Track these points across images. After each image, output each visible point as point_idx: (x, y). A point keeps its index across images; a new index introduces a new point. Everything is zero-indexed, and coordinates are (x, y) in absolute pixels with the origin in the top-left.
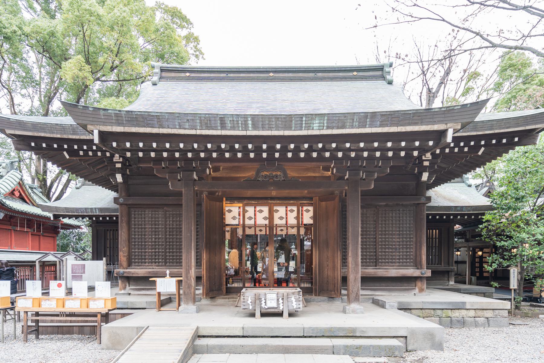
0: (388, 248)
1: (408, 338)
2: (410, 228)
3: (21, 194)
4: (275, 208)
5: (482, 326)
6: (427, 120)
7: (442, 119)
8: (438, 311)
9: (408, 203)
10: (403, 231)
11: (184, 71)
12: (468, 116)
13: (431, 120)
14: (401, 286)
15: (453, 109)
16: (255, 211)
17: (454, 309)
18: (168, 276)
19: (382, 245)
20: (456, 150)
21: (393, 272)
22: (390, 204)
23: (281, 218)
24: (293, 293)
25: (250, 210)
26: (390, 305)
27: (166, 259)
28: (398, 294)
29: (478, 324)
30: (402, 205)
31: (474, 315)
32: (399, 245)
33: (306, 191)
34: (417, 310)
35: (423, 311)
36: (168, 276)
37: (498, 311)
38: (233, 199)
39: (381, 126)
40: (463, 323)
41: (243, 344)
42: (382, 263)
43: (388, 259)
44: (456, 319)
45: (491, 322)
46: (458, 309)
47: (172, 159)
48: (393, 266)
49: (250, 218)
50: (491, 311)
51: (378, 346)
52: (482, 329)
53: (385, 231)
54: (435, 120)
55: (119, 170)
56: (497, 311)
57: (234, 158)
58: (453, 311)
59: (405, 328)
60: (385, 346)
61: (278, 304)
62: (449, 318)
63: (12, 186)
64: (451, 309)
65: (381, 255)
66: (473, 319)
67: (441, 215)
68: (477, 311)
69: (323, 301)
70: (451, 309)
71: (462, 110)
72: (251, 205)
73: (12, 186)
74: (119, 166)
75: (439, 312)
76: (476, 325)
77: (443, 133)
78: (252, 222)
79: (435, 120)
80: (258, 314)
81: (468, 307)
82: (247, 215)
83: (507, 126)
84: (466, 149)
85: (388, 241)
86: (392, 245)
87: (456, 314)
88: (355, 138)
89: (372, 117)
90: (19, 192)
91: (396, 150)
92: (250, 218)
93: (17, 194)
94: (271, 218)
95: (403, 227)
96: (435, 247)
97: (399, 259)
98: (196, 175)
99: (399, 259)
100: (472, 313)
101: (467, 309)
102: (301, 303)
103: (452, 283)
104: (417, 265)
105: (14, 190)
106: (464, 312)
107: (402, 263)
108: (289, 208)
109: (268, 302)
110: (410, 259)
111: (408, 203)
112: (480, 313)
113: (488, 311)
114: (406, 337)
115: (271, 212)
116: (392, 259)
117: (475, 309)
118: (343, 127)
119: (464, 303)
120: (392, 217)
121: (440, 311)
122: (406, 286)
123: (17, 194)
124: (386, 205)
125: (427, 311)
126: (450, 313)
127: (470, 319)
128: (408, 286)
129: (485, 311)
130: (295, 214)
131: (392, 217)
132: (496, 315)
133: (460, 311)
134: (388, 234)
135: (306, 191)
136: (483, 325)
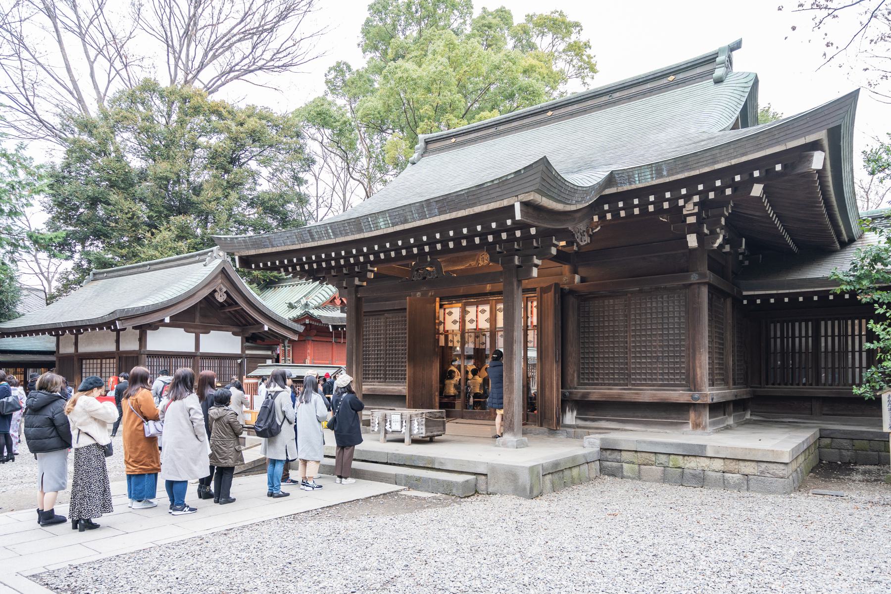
0: (645, 357)
2: (679, 324)
5: (735, 488)
6: (484, 198)
7: (499, 194)
8: (662, 456)
9: (675, 284)
10: (668, 329)
11: (544, 111)
12: (528, 185)
13: (489, 197)
14: (666, 418)
15: (507, 180)
17: (689, 456)
19: (635, 352)
20: (712, 195)
21: (647, 395)
22: (646, 288)
24: (416, 415)
25: (472, 310)
26: (589, 443)
27: (385, 374)
28: (643, 429)
29: (729, 483)
30: (665, 288)
31: (722, 468)
32: (662, 352)
33: (419, 294)
35: (639, 454)
37: (766, 464)
38: (452, 298)
39: (441, 213)
40: (701, 480)
41: (398, 472)
42: (635, 379)
43: (645, 374)
45: (751, 483)
46: (695, 456)
47: (339, 267)
48: (653, 385)
50: (753, 464)
51: (437, 480)
52: (735, 494)
53: (640, 330)
54: (493, 196)
55: (692, 229)
56: (764, 465)
57: (399, 256)
58: (686, 458)
59: (484, 463)
60: (444, 481)
62: (680, 470)
63: (331, 293)
64: (684, 456)
65: (634, 368)
66: (720, 474)
67: (808, 296)
68: (728, 462)
69: (543, 434)
70: (684, 456)
71: (517, 178)
72: (471, 304)
73: (331, 293)
74: (691, 220)
75: (663, 459)
76: (725, 485)
77: (512, 207)
78: (473, 326)
79: (493, 196)
80: (407, 440)
81: (710, 453)
82: (468, 318)
83: (741, 152)
84: (728, 192)
85: (645, 346)
86: (651, 352)
87: (692, 464)
88: (416, 232)
89: (427, 206)
91: (643, 206)
92: (471, 321)
95: (668, 324)
97: (662, 374)
99: (662, 374)
100: (718, 465)
101: (711, 458)
102: (424, 427)
103: (748, 416)
105: (335, 298)
106: (703, 463)
107: (645, 380)
108: (480, 308)
109: (393, 424)
110: (681, 374)
111: (675, 284)
112: (732, 466)
113: (747, 464)
115: (464, 312)
116: (651, 374)
117: (724, 459)
118: (406, 221)
119: (703, 447)
120: (651, 309)
121: (665, 456)
122: (675, 419)
124: (641, 291)
125: (643, 454)
128: (679, 418)
129: (742, 464)
130: (487, 315)
131: (651, 309)
132: (762, 472)
133: (698, 459)
134: (645, 336)
135: (419, 294)
136: (738, 487)
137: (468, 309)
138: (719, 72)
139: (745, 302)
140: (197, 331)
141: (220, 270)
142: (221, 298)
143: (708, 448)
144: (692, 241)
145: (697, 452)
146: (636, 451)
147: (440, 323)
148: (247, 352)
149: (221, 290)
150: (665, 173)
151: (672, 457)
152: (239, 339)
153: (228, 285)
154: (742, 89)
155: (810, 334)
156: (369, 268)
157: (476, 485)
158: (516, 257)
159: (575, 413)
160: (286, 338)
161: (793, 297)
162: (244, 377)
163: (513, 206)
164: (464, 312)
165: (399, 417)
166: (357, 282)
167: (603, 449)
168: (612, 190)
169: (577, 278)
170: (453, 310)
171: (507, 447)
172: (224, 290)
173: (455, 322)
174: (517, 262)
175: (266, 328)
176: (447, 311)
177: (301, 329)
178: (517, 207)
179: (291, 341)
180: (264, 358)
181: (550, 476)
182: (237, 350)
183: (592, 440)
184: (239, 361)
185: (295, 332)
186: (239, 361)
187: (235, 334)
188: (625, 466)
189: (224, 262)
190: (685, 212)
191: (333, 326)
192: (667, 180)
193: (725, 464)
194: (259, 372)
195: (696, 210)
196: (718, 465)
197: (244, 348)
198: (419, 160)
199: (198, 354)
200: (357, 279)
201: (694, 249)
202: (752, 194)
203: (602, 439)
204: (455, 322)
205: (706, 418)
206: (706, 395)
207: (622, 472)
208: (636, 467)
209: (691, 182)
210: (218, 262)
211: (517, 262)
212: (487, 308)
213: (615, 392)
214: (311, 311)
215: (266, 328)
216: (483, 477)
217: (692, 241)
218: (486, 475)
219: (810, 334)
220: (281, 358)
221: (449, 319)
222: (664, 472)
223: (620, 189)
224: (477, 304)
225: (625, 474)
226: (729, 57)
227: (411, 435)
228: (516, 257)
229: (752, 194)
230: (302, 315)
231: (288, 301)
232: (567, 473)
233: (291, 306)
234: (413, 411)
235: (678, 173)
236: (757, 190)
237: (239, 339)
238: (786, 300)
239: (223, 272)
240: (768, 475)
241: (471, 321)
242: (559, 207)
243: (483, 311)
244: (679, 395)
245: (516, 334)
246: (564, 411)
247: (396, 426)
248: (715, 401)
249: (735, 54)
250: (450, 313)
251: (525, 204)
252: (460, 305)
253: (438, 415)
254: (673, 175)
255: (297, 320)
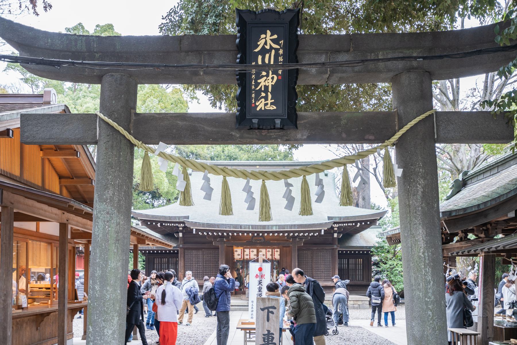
9: (480, 274)
82: (245, 253)
92: (247, 255)
108: (267, 250)
112: (356, 302)
115: (258, 252)
124: (317, 249)
130: (270, 253)
136: (357, 308)
137: (245, 250)
161: (346, 251)
164: (258, 252)
173: (239, 255)
204: (239, 255)
212: (255, 250)
241: (247, 255)
243: (253, 251)
246: (469, 239)
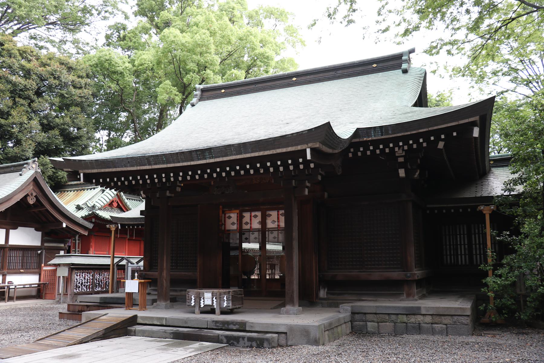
1: (288, 334)
3: (118, 204)
4: (268, 212)
8: (393, 316)
16: (278, 215)
17: (410, 314)
18: (136, 278)
21: (376, 275)
23: (274, 222)
25: (247, 215)
29: (435, 331)
34: (370, 315)
36: (136, 278)
38: (231, 207)
40: (418, 329)
44: (412, 325)
46: (414, 314)
49: (247, 223)
50: (449, 317)
55: (402, 165)
56: (455, 318)
59: (285, 325)
61: (213, 303)
62: (405, 324)
66: (430, 325)
68: (434, 317)
70: (407, 315)
73: (111, 198)
74: (401, 160)
75: (393, 317)
76: (433, 332)
80: (218, 311)
81: (423, 312)
90: (117, 202)
92: (247, 223)
93: (115, 204)
94: (263, 222)
96: (476, 244)
98: (144, 193)
100: (428, 319)
101: (424, 315)
104: (404, 267)
105: (113, 201)
106: (420, 318)
108: (253, 214)
109: (206, 300)
112: (437, 319)
113: (446, 317)
114: (286, 333)
115: (240, 218)
119: (419, 308)
123: (115, 204)
125: (380, 315)
126: (405, 319)
127: (427, 325)
129: (443, 318)
130: (259, 219)
132: (455, 322)
136: (441, 333)
138: (404, 66)
139: (428, 212)
140: (7, 227)
141: (33, 179)
142: (31, 201)
143: (422, 309)
144: (402, 173)
145: (415, 312)
146: (376, 314)
147: (223, 224)
148: (46, 244)
149: (32, 194)
150: (390, 132)
151: (400, 316)
152: (39, 234)
153: (37, 190)
154: (419, 78)
155: (466, 233)
156: (178, 184)
157: (282, 340)
158: (294, 181)
159: (326, 290)
160: (78, 233)
162: (43, 265)
163: (305, 150)
164: (240, 218)
165: (210, 294)
166: (168, 194)
167: (353, 313)
168: (357, 140)
169: (326, 195)
170: (232, 215)
171: (290, 314)
172: (34, 194)
173: (233, 224)
174: (294, 184)
175: (64, 225)
176: (227, 215)
177: (90, 226)
178: (308, 151)
179: (81, 236)
180: (61, 249)
181: (327, 332)
182: (38, 243)
183: (346, 307)
184: (39, 252)
185: (85, 228)
186: (39, 252)
187: (37, 230)
188: (369, 324)
189: (36, 172)
190: (397, 155)
191: (121, 225)
192: (391, 136)
193: (433, 319)
194: (55, 261)
195: (404, 154)
196: (428, 319)
197: (43, 242)
198: (197, 103)
199: (7, 246)
200: (168, 192)
201: (403, 178)
202: (438, 147)
203: (352, 306)
205: (415, 290)
206: (415, 274)
207: (367, 328)
208: (376, 324)
209: (405, 139)
210: (32, 172)
211: (294, 184)
212: (259, 214)
213: (355, 273)
214: (98, 212)
215: (64, 225)
216: (284, 335)
217: (402, 173)
218: (286, 333)
219: (466, 233)
220: (72, 249)
221: (229, 222)
222: (395, 327)
223: (361, 140)
224: (251, 211)
225: (369, 329)
226: (409, 57)
227: (220, 308)
228: (294, 181)
229: (438, 147)
230: (89, 215)
231: (81, 202)
232: (335, 329)
233: (79, 208)
234: (222, 291)
235: (398, 133)
236: (441, 145)
237: (39, 234)
238: (444, 211)
239: (35, 181)
240: (459, 324)
242: (329, 151)
243: (256, 216)
244: (396, 275)
245: (294, 234)
247: (208, 302)
248: (419, 278)
249: (411, 55)
250: (230, 217)
251: (312, 150)
252: (238, 211)
253: (239, 292)
254: (395, 134)
255: (85, 218)
